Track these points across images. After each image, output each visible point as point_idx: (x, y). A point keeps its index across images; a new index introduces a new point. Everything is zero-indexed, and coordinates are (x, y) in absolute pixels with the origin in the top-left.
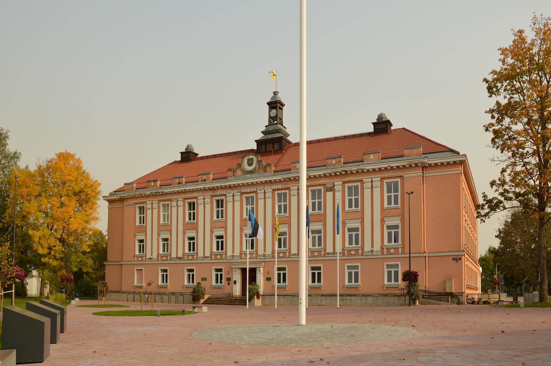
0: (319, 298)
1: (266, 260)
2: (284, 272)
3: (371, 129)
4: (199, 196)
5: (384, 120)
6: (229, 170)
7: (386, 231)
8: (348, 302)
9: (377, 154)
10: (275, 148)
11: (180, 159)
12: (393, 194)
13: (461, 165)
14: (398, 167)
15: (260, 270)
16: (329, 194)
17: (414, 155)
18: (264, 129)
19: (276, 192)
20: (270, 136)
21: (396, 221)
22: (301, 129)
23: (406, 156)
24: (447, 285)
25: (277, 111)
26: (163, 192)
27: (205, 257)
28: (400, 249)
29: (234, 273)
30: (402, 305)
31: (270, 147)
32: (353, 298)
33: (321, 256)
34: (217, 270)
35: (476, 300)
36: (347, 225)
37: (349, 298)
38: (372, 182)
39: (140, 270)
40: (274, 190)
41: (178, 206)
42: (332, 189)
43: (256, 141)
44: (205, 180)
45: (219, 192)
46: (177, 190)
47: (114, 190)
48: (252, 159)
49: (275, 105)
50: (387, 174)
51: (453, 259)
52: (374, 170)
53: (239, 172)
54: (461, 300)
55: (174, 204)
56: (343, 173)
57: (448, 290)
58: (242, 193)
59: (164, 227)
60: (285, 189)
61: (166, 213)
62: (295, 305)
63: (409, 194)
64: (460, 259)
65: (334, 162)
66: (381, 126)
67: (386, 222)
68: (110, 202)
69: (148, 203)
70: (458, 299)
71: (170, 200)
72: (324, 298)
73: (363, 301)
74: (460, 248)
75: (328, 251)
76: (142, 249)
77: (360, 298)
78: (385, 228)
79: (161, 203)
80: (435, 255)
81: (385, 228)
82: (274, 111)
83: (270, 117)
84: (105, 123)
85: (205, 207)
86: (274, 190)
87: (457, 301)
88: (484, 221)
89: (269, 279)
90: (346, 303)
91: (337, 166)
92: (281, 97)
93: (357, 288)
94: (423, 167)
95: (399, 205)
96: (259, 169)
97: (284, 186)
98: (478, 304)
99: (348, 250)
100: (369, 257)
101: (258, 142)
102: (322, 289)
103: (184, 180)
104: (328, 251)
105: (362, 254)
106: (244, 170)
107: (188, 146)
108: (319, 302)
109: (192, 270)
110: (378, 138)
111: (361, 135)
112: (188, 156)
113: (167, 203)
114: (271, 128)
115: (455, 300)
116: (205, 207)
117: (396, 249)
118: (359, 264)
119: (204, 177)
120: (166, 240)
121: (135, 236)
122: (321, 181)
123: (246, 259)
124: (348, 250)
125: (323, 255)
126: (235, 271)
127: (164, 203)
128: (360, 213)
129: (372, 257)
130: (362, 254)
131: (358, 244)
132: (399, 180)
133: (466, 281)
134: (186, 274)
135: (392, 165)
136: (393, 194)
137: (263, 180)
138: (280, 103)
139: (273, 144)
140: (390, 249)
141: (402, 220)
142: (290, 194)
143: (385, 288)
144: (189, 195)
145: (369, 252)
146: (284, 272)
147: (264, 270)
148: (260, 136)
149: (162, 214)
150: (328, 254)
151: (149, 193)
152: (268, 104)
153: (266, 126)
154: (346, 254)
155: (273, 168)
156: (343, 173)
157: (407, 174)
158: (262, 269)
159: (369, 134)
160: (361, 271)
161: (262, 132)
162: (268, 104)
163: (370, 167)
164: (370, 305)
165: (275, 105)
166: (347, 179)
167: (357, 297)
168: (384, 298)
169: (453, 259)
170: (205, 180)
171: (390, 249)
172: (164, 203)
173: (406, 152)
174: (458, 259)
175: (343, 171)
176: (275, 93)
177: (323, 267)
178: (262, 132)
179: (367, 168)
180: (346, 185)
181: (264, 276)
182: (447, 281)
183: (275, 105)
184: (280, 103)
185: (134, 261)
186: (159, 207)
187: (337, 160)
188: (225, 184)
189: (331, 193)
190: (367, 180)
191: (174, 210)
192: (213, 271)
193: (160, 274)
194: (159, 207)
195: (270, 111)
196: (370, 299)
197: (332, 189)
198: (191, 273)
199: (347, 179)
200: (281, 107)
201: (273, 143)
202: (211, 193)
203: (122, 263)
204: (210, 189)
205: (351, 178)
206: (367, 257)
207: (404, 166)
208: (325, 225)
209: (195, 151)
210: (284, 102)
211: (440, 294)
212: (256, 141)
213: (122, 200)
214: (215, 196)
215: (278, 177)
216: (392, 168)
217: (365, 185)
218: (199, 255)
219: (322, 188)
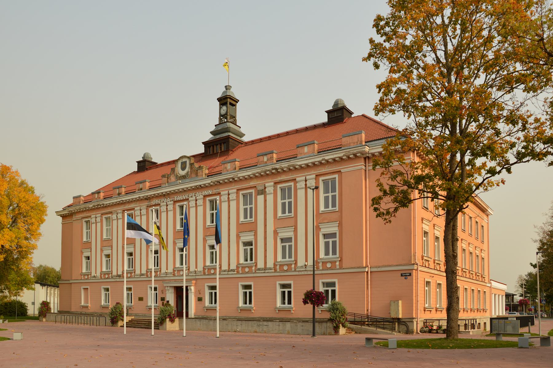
0: (235, 323)
1: (197, 277)
2: (289, 290)
3: (324, 119)
4: (136, 207)
5: (340, 106)
6: (163, 176)
7: (322, 241)
8: (265, 328)
9: (312, 145)
10: (223, 150)
11: (136, 170)
12: (330, 195)
13: (413, 152)
14: (334, 160)
15: (191, 289)
16: (261, 198)
17: (354, 143)
18: (213, 128)
19: (208, 199)
20: (218, 137)
21: (333, 228)
22: (252, 125)
23: (345, 146)
24: (392, 308)
25: (227, 107)
26: (103, 204)
27: (142, 275)
28: (338, 263)
29: (167, 292)
30: (324, 334)
31: (217, 149)
32: (270, 323)
33: (252, 273)
34: (283, 286)
35: (435, 328)
36: (280, 235)
37: (265, 323)
38: (306, 181)
39: (86, 289)
40: (205, 196)
41: (117, 219)
42: (263, 192)
43: (203, 143)
44: (141, 189)
45: (154, 202)
46: (116, 201)
47: (68, 204)
48: (186, 162)
49: (227, 101)
50: (206, 193)
51: (402, 276)
52: (307, 166)
53: (173, 178)
54: (410, 328)
55: (114, 216)
56: (274, 171)
57: (393, 315)
58: (175, 202)
59: (107, 242)
60: (215, 195)
61: (109, 227)
62: (211, 330)
63: (313, 190)
64: (410, 275)
65: (265, 159)
66: (336, 114)
67: (322, 230)
68: (64, 217)
69: (92, 216)
70: (407, 327)
71: (111, 213)
72: (239, 322)
73: (281, 328)
74: (411, 260)
75: (259, 267)
76: (88, 267)
77: (277, 323)
78: (279, 241)
79: (104, 216)
80: (379, 269)
81: (321, 237)
82: (224, 108)
83: (221, 115)
84: (76, 136)
85: (141, 219)
86: (205, 196)
87: (406, 329)
88: (390, 221)
89: (200, 299)
90: (262, 330)
91: (268, 163)
92: (235, 93)
93: (249, 310)
94: (365, 158)
95: (337, 208)
96: (191, 173)
97: (215, 191)
98: (437, 333)
99: (280, 265)
100: (303, 273)
101: (207, 144)
102: (253, 311)
103: (123, 190)
104: (259, 267)
105: (295, 271)
106: (177, 175)
107: (144, 155)
108: (235, 328)
109: (249, 287)
110: (337, 128)
111: (315, 127)
112: (145, 165)
113: (109, 215)
114: (220, 127)
115: (403, 328)
116: (141, 219)
117: (333, 263)
118: (336, 281)
119: (141, 186)
120: (108, 256)
121: (82, 253)
122: (252, 183)
123: (151, 277)
124: (280, 265)
125: (254, 271)
126: (168, 290)
127: (106, 216)
128: (293, 219)
129: (306, 273)
130: (341, 268)
131: (291, 258)
132: (336, 176)
133: (420, 302)
134: (279, 291)
135: (327, 158)
136: (330, 195)
137: (193, 185)
138: (230, 98)
139: (221, 144)
140: (326, 262)
141: (340, 226)
142: (220, 200)
143: (277, 312)
144: (127, 207)
145: (302, 267)
146: (333, 288)
147: (195, 289)
148: (209, 137)
149: (105, 228)
150: (259, 269)
151: (91, 206)
152: (219, 100)
153: (216, 126)
154: (278, 270)
155: (207, 172)
156: (274, 171)
157: (346, 168)
158: (193, 288)
159: (324, 125)
160: (294, 290)
161: (211, 133)
162: (219, 100)
163: (302, 162)
164: (288, 333)
165: (227, 101)
166: (279, 179)
167: (274, 323)
168: (304, 324)
169: (402, 276)
170: (141, 189)
171: (326, 262)
172: (106, 216)
173: (345, 140)
174: (406, 275)
175: (273, 169)
176: (227, 88)
177: (254, 285)
178: (211, 133)
179: (299, 163)
180: (279, 186)
181: (195, 296)
182: (392, 304)
183: (225, 101)
184: (230, 98)
185: (82, 279)
186: (102, 220)
187: (269, 156)
188: (158, 192)
189: (263, 196)
190: (300, 178)
191: (115, 222)
192: (278, 287)
193: (241, 291)
194: (102, 220)
195: (220, 108)
196: (288, 325)
197: (263, 192)
198: (248, 291)
199: (279, 179)
200: (234, 103)
201: (221, 144)
202: (146, 203)
203: (71, 282)
204: (148, 199)
205: (284, 177)
206: (300, 273)
207: (341, 158)
208: (256, 235)
209: (153, 160)
210: (237, 97)
211: (384, 320)
212: (203, 143)
213: (71, 215)
214: (151, 206)
215: (208, 181)
216: (327, 161)
217: (298, 185)
218: (136, 273)
219: (253, 191)
